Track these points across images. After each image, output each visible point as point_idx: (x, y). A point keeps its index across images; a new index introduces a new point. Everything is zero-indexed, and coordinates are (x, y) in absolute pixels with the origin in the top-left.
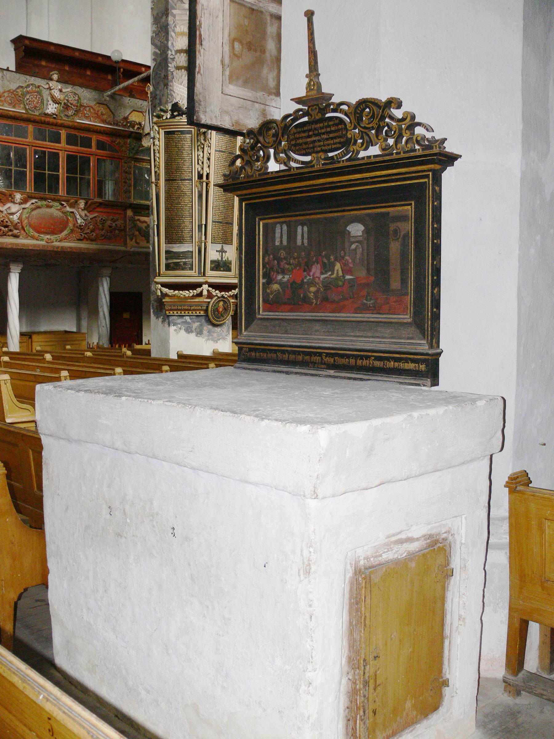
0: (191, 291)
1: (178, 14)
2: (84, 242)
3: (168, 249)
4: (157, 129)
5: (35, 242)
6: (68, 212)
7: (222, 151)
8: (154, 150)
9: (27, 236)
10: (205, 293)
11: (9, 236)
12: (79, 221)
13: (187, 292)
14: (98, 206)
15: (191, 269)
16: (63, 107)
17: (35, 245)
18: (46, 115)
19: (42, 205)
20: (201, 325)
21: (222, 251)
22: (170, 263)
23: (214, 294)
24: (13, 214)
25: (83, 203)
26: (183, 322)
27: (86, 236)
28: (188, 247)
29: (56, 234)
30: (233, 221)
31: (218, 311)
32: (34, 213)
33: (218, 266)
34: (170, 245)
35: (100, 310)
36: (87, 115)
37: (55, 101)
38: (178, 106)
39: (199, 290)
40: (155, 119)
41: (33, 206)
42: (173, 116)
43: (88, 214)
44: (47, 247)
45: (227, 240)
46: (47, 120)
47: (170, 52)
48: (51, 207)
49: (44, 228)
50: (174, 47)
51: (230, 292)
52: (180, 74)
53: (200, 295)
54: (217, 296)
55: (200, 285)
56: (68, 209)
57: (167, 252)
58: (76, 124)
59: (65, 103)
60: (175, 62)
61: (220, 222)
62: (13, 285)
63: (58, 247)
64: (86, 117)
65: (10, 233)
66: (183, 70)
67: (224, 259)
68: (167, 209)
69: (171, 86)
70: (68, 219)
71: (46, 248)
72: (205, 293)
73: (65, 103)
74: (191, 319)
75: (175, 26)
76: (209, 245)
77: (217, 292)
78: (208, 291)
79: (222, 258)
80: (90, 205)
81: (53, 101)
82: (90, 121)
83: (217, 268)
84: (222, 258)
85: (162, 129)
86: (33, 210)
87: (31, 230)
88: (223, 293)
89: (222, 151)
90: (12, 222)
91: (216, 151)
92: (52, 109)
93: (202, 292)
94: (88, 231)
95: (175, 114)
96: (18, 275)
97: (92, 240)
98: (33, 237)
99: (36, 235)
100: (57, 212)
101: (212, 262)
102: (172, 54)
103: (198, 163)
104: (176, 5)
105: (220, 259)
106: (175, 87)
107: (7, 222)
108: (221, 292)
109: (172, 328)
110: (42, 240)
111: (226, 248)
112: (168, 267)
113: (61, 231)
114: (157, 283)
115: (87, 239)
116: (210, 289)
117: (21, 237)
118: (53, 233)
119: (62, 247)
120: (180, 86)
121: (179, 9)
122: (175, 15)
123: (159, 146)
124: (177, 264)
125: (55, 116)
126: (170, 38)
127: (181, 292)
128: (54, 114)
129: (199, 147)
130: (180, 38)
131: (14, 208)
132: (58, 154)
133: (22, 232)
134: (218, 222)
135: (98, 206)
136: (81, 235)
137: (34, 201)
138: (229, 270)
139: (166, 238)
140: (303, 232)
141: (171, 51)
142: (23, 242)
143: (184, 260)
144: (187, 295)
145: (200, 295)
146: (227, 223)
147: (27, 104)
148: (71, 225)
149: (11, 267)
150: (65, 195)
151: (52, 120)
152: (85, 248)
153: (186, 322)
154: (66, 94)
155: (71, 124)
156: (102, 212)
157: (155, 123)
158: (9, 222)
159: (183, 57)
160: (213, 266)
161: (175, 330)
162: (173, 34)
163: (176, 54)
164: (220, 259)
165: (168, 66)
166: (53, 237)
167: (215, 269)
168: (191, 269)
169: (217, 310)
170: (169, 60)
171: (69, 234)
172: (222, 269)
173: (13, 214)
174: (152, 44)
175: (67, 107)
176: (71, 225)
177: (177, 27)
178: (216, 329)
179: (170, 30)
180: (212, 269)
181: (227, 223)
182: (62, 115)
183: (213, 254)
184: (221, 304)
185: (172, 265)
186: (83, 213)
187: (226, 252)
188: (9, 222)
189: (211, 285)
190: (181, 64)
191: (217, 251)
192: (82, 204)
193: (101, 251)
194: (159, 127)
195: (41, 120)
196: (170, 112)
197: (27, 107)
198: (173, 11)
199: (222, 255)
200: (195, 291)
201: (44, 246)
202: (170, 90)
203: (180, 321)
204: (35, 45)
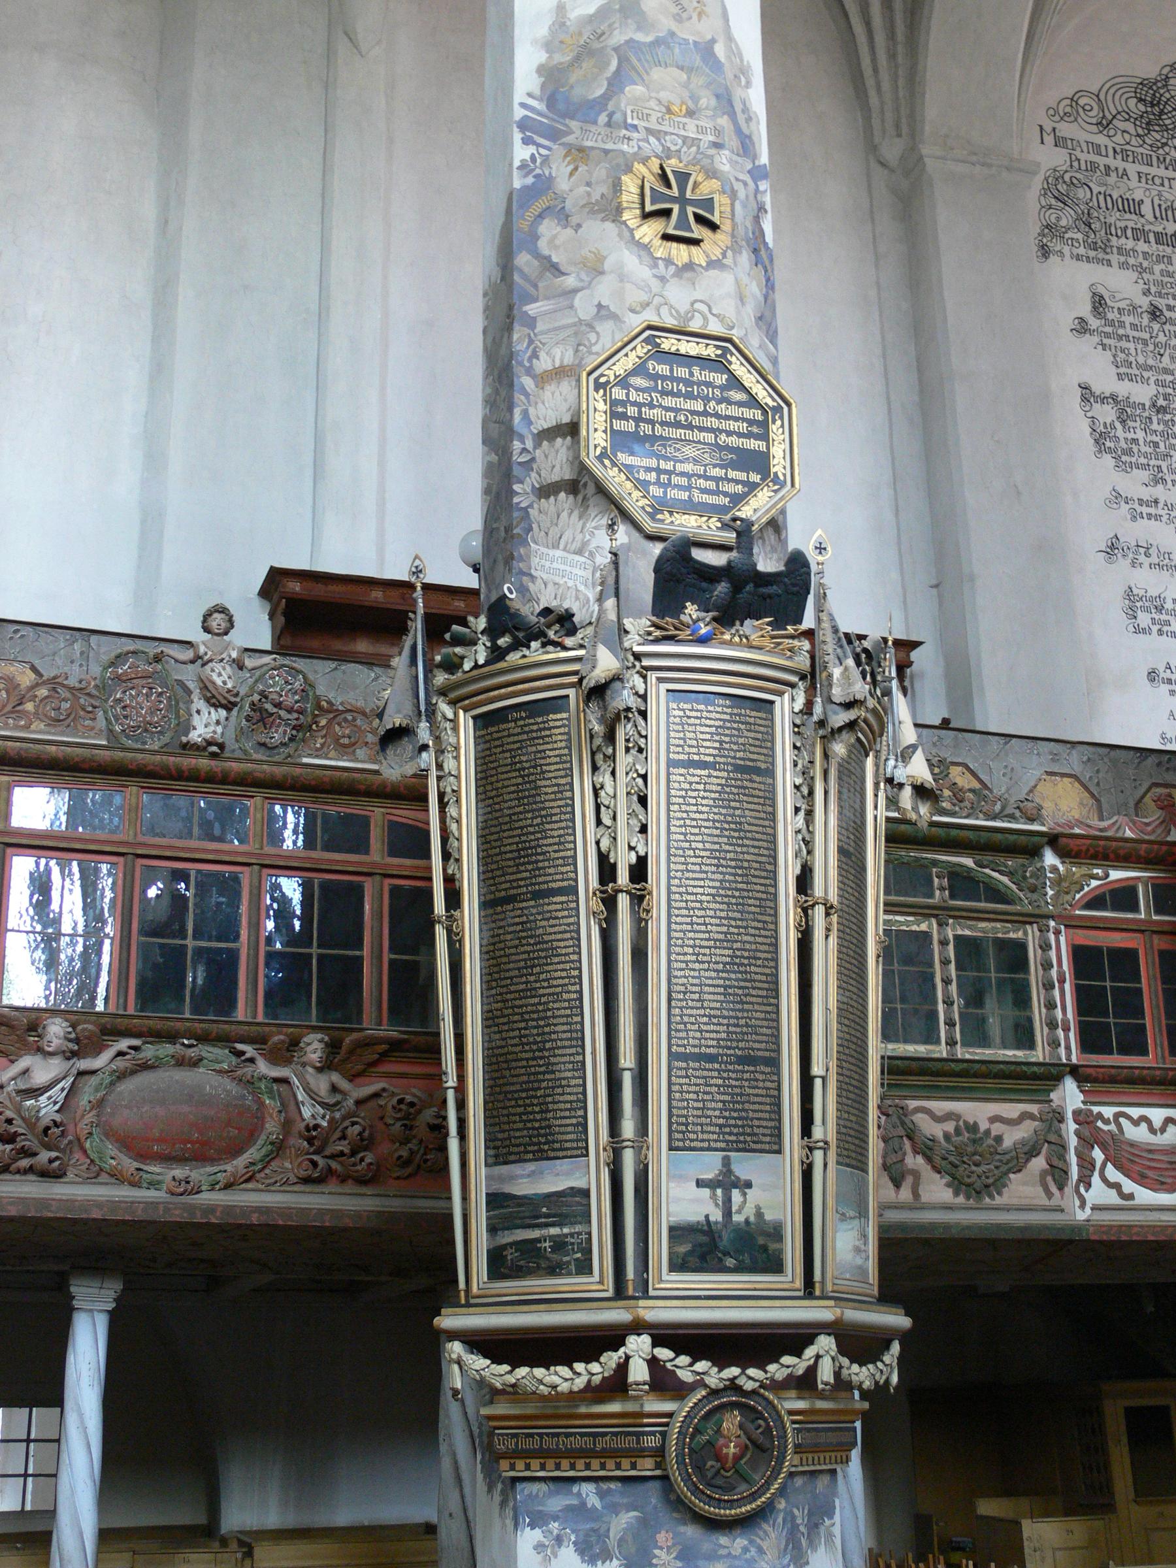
0: (579, 1367)
1: (545, 313)
2: (332, 1186)
3: (496, 1187)
4: (449, 712)
5: (124, 1193)
6: (265, 1077)
7: (703, 765)
8: (441, 795)
9: (96, 1173)
10: (639, 1372)
11: (18, 1172)
12: (307, 1112)
13: (564, 1371)
14: (384, 1055)
15: (585, 1267)
16: (248, 719)
17: (114, 1205)
18: (188, 748)
19: (157, 1058)
20: (644, 1522)
21: (727, 1182)
22: (504, 1247)
23: (686, 1376)
24: (35, 1092)
25: (317, 1045)
26: (569, 1509)
27: (334, 1165)
28: (569, 1174)
29: (212, 1161)
30: (778, 1051)
31: (719, 1457)
32: (127, 1087)
33: (702, 1248)
34: (504, 1169)
35: (443, 1448)
36: (346, 741)
37: (214, 701)
38: (507, 608)
39: (611, 1359)
40: (441, 678)
41: (121, 1063)
42: (497, 654)
43: (344, 1084)
44: (167, 1210)
45: (753, 1132)
46: (187, 762)
47: (517, 445)
48: (195, 1063)
49: (160, 1141)
50: (531, 423)
51: (772, 1368)
52: (552, 509)
53: (617, 1384)
54: (701, 1384)
55: (613, 1337)
56: (263, 1067)
57: (495, 1200)
58: (297, 771)
59: (253, 704)
60: (533, 475)
61: (711, 1058)
62: (80, 1358)
63: (211, 1209)
64: (344, 746)
65: (24, 1163)
66: (562, 495)
67: (736, 1218)
68: (490, 1019)
69: (521, 559)
70: (262, 1104)
71: (160, 1216)
72: (639, 1372)
73: (253, 704)
74: (601, 1495)
75: (535, 355)
76: (661, 1159)
77: (702, 1366)
78: (653, 1362)
79: (728, 1213)
80: (351, 1052)
81: (208, 700)
82: (356, 760)
83: (703, 1257)
84: (728, 1213)
85: (466, 710)
86: (122, 1076)
87: (111, 1149)
88: (734, 1371)
89: (703, 765)
90: (31, 1123)
91: (671, 764)
92: (205, 724)
93: (623, 1367)
94: (344, 1147)
95: (503, 641)
96: (102, 1322)
97: (362, 1181)
98: (118, 1177)
99: (129, 1164)
100: (216, 1079)
101: (677, 1232)
102: (524, 450)
103: (599, 822)
104: (536, 286)
105: (717, 1216)
106: (535, 561)
107: (9, 1121)
108: (722, 1366)
109: (528, 1538)
110: (153, 1185)
111: (745, 1166)
112: (499, 1266)
113: (235, 1151)
114: (453, 1335)
115: (343, 1180)
116: (664, 1353)
117: (70, 1176)
118: (199, 1157)
119: (228, 1210)
120: (551, 552)
121: (547, 298)
122: (534, 319)
123: (458, 777)
124: (529, 1248)
125: (214, 749)
126: (519, 397)
127: (539, 1372)
128: (210, 743)
129: (599, 757)
130: (550, 388)
131: (43, 1071)
132: (235, 878)
133: (78, 1155)
134: (699, 1057)
135: (384, 1055)
136: (315, 1164)
137: (124, 1044)
138: (775, 1265)
139: (490, 1140)
140: (710, 993)
141: (522, 439)
142: (77, 1193)
143: (554, 1231)
144: (564, 1387)
145: (617, 1384)
146: (747, 1060)
147: (117, 719)
148: (272, 1127)
149: (72, 1289)
150: (260, 1018)
151: (204, 763)
152: (358, 1215)
153: (580, 1510)
154: (258, 673)
155: (279, 771)
156: (402, 1076)
157: (443, 692)
158: (18, 1122)
159: (563, 451)
160: (683, 1249)
161: (539, 1547)
162: (528, 382)
163: (538, 445)
164: (717, 1216)
165: (513, 493)
166: (198, 1174)
167: (694, 1261)
168: (585, 1267)
169: (712, 1448)
170: (517, 471)
171: (267, 1160)
172: (730, 1262)
173: (35, 1092)
174: (484, 442)
175: (261, 716)
176: (272, 1127)
177: (542, 355)
178: (723, 1540)
179: (517, 369)
180: (678, 1265)
181: (747, 1060)
182: (248, 746)
183: (682, 1198)
184: (731, 1422)
185: (510, 1254)
186: (321, 1084)
187: (749, 1185)
188: (18, 1122)
189: (665, 1336)
190: (555, 477)
191: (700, 1184)
192: (314, 1047)
193: (391, 1217)
194: (453, 703)
195: (165, 767)
196: (484, 639)
197: (118, 728)
198: (526, 308)
199: (728, 1201)
200: (595, 1367)
201: (154, 1205)
202: (522, 573)
203: (557, 1503)
204: (320, 591)
